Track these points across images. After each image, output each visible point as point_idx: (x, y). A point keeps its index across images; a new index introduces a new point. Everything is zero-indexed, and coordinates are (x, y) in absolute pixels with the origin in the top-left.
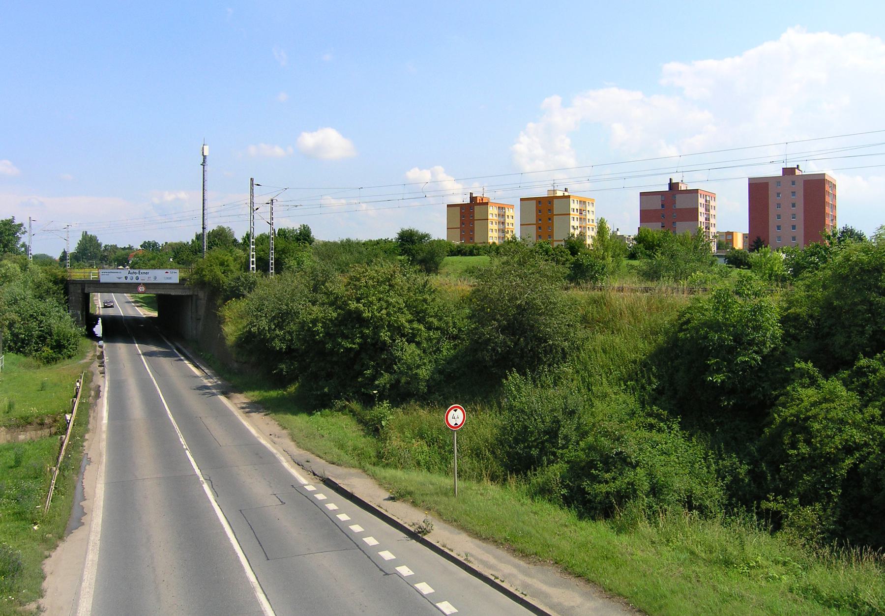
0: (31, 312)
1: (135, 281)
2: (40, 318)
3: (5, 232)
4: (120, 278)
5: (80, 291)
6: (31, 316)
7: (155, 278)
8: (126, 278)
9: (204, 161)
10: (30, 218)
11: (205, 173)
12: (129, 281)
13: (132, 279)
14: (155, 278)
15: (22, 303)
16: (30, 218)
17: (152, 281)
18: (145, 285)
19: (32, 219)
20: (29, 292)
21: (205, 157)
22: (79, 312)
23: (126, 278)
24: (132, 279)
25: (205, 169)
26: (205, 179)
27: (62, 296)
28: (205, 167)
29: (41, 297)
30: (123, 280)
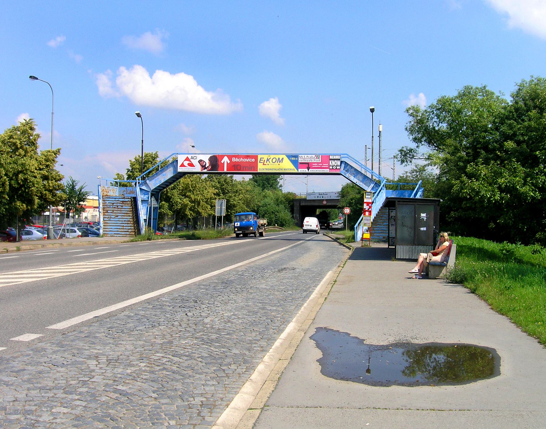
0: (272, 210)
1: (321, 198)
2: (276, 213)
3: (271, 179)
4: (315, 197)
5: (298, 205)
6: (272, 212)
7: (330, 197)
8: (318, 197)
9: (380, 134)
10: (366, 146)
11: (381, 141)
12: (319, 198)
13: (320, 197)
14: (330, 197)
15: (268, 206)
16: (366, 146)
17: (329, 198)
18: (326, 200)
19: (367, 147)
20: (272, 201)
21: (380, 132)
22: (298, 215)
23: (318, 197)
24: (320, 197)
25: (381, 139)
26: (381, 145)
27: (287, 205)
28: (381, 138)
29: (278, 205)
30: (317, 198)
